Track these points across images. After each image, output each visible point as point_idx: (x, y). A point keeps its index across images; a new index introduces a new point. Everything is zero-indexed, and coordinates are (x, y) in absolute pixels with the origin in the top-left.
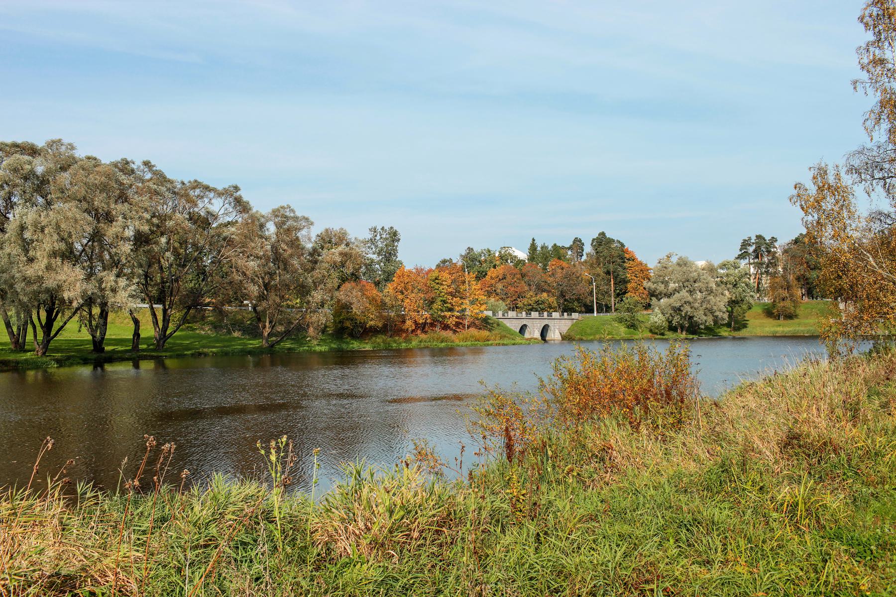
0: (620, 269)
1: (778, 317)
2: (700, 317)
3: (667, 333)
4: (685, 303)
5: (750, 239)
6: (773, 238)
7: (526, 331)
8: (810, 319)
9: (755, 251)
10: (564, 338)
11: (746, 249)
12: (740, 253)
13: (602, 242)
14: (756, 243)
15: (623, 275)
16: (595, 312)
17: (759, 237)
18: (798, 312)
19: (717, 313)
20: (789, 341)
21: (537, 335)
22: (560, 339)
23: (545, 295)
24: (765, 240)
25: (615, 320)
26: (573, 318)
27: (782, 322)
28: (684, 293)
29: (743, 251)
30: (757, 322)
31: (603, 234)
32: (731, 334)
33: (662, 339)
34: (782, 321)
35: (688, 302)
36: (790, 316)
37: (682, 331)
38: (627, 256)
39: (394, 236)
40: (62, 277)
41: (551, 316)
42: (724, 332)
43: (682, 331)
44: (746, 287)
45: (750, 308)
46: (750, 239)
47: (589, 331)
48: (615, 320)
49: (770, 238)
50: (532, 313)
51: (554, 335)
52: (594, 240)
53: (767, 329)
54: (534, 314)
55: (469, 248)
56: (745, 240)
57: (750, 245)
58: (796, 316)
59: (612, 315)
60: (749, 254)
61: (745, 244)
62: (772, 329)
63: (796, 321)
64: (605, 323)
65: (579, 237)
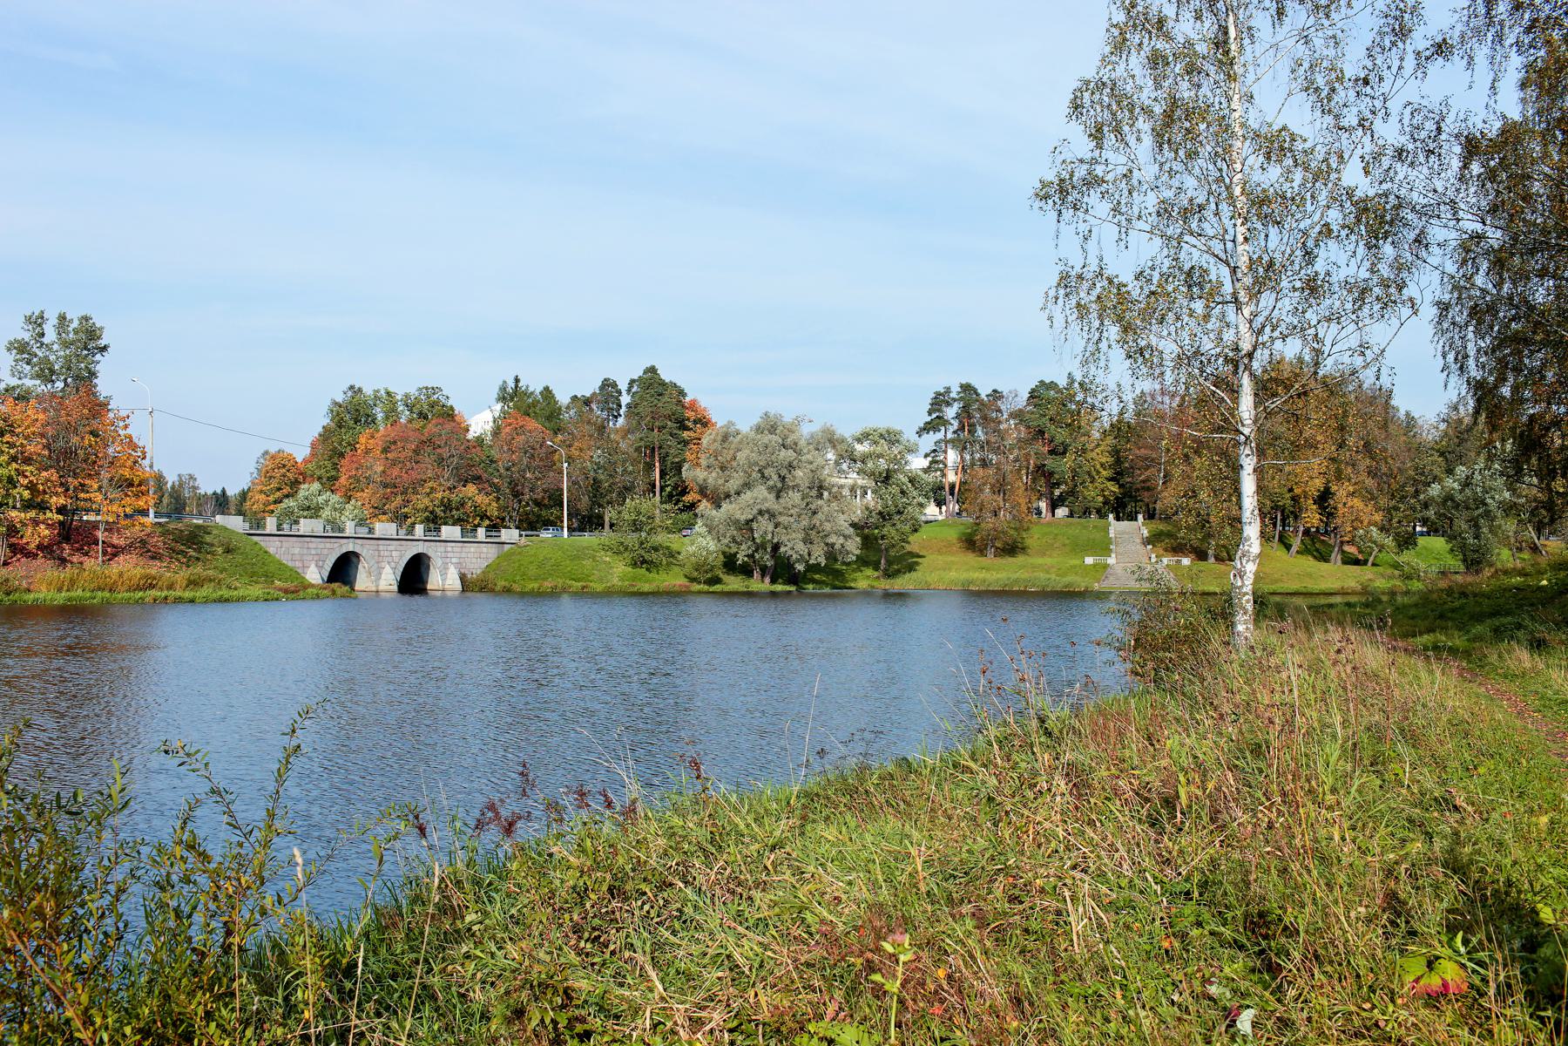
0: (672, 442)
1: (982, 552)
2: (793, 547)
3: (725, 578)
4: (761, 513)
5: (948, 390)
6: (995, 391)
7: (360, 566)
8: (1050, 556)
9: (958, 416)
10: (467, 584)
11: (940, 411)
12: (929, 419)
13: (651, 383)
14: (961, 399)
15: (676, 456)
16: (566, 529)
17: (967, 388)
18: (1028, 542)
19: (833, 539)
20: (854, 602)
21: (389, 579)
22: (459, 587)
23: (471, 489)
24: (978, 395)
25: (606, 548)
26: (503, 539)
27: (990, 561)
28: (760, 495)
29: (934, 416)
30: (940, 559)
31: (652, 370)
32: (875, 584)
33: (888, 596)
34: (990, 559)
35: (768, 511)
36: (1012, 549)
37: (763, 576)
38: (689, 414)
39: (88, 340)
40: (1248, 584)
41: (475, 537)
42: (864, 580)
43: (763, 576)
44: (910, 485)
45: (916, 531)
46: (948, 390)
47: (533, 571)
48: (606, 548)
49: (989, 391)
50: (444, 528)
51: (443, 578)
52: (632, 382)
53: (953, 575)
54: (450, 531)
55: (352, 387)
56: (938, 394)
57: (948, 404)
58: (1024, 549)
59: (606, 536)
60: (946, 423)
61: (940, 401)
62: (964, 576)
63: (1020, 559)
64: (578, 555)
65: (613, 377)
